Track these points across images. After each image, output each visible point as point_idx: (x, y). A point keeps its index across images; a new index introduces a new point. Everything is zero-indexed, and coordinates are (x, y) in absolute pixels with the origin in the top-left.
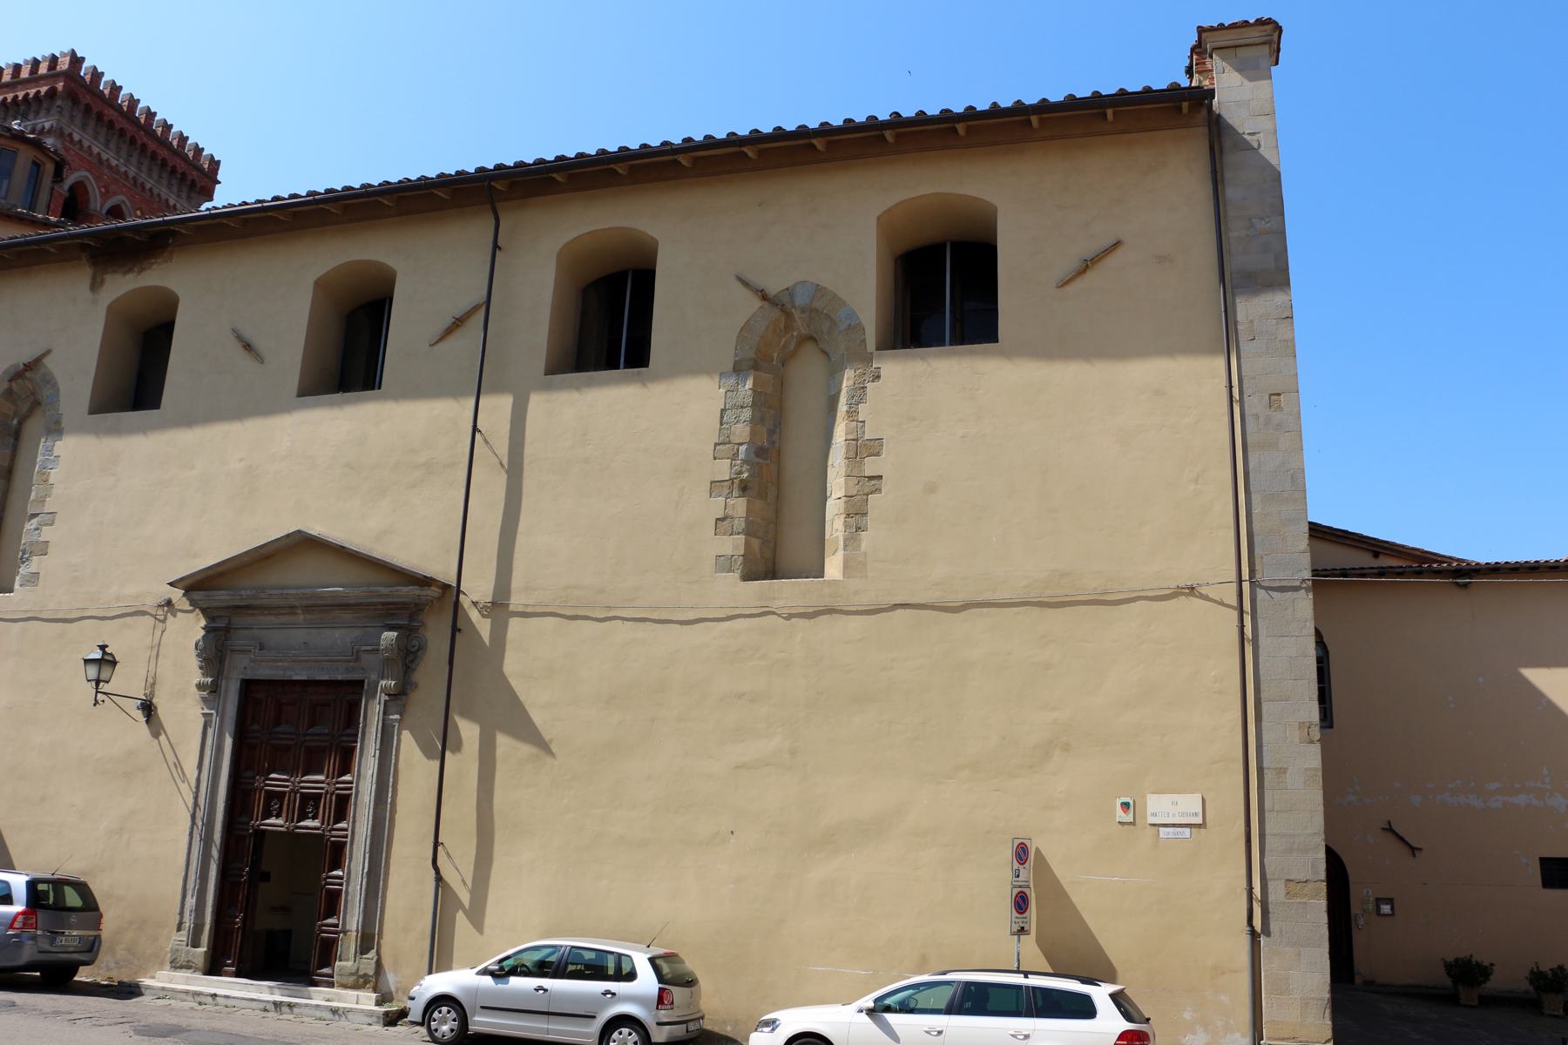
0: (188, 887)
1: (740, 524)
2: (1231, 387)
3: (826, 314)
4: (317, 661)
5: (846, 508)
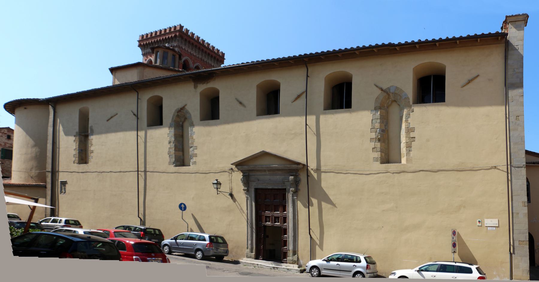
1: (379, 149)
2: (506, 114)
3: (399, 95)
4: (273, 184)
5: (406, 146)
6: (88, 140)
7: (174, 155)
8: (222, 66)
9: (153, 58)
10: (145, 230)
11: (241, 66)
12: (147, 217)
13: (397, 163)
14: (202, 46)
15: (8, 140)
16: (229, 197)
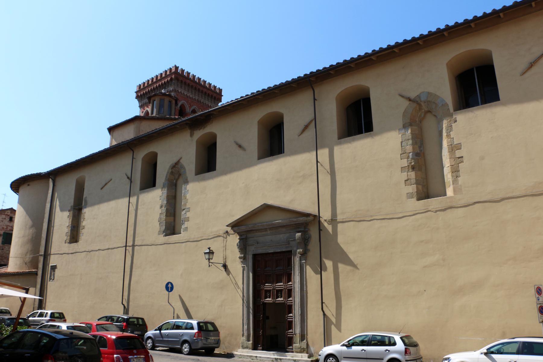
0: (244, 322)
1: (413, 181)
5: (451, 170)
6: (81, 214)
7: (165, 222)
8: (220, 104)
9: (149, 109)
10: (127, 321)
11: (240, 100)
12: (130, 303)
13: (440, 197)
14: (198, 85)
15: (10, 223)
16: (223, 269)
